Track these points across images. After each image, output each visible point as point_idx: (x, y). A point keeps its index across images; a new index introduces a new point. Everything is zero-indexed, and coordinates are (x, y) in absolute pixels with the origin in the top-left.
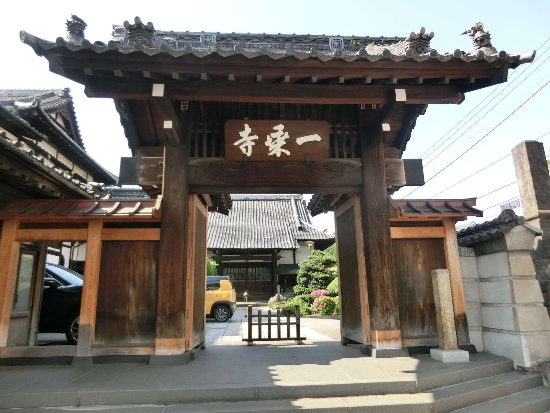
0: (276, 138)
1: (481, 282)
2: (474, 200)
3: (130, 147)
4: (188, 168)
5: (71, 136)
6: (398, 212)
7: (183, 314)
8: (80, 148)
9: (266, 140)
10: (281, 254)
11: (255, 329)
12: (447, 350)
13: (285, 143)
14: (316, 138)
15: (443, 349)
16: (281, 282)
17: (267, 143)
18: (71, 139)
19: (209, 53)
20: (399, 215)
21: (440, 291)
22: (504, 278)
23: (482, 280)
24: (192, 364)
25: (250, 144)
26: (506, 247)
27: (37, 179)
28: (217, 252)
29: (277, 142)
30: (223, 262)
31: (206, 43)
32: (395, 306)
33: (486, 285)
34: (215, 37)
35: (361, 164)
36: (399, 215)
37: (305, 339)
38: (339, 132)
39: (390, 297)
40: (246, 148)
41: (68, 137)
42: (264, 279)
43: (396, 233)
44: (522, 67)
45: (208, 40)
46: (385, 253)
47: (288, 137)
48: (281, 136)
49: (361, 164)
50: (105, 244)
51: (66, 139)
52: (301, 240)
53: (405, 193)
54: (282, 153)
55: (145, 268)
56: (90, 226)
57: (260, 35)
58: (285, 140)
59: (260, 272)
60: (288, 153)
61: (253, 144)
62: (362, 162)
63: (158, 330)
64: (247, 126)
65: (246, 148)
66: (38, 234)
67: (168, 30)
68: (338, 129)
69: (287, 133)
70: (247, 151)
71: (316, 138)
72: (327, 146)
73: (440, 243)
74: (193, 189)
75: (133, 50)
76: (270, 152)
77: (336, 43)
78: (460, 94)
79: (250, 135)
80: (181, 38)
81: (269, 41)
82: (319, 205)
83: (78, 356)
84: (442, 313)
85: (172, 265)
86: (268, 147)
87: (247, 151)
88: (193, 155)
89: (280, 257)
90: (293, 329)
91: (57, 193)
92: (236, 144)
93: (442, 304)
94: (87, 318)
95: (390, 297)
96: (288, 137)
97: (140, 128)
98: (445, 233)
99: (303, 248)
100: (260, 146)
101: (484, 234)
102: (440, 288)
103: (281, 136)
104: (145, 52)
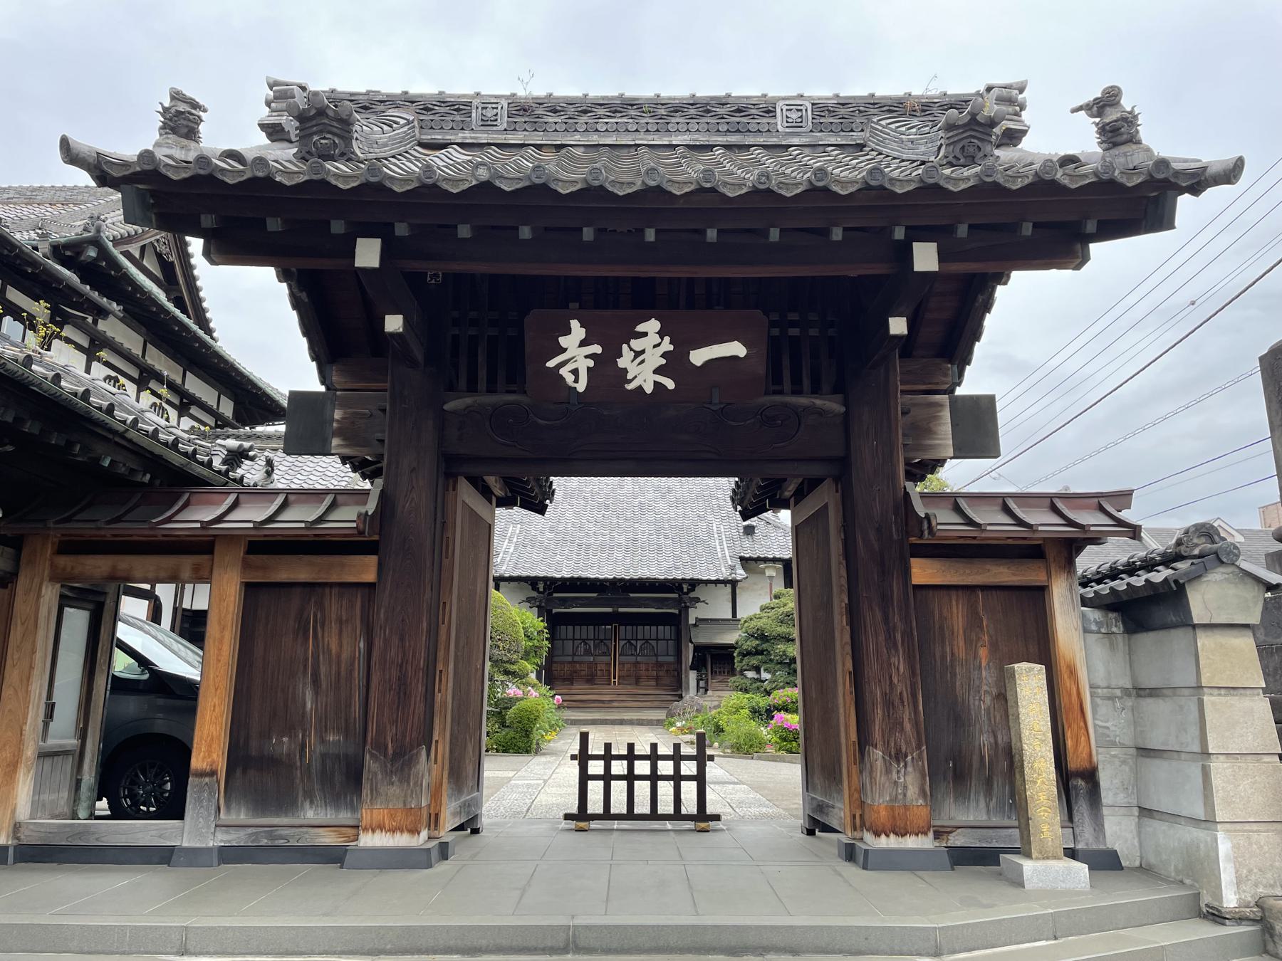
0: (643, 352)
1: (1139, 696)
2: (1124, 497)
3: (313, 359)
4: (442, 419)
5: (179, 303)
6: (926, 526)
7: (424, 752)
8: (201, 333)
9: (621, 356)
10: (699, 592)
11: (595, 788)
12: (1038, 859)
13: (663, 361)
14: (736, 349)
15: (1028, 855)
16: (698, 665)
17: (622, 363)
18: (177, 312)
19: (474, 183)
20: (926, 532)
21: (1022, 717)
22: (1186, 692)
23: (1141, 692)
24: (442, 868)
25: (584, 365)
26: (1191, 618)
27: (99, 448)
28: (541, 586)
29: (645, 360)
30: (554, 611)
31: (486, 123)
32: (919, 747)
33: (1149, 704)
34: (505, 106)
35: (843, 409)
36: (926, 532)
37: (717, 818)
38: (794, 332)
39: (908, 726)
40: (575, 372)
41: (170, 306)
42: (656, 655)
43: (923, 572)
44: (1214, 194)
45: (489, 113)
46: (896, 619)
47: (671, 348)
48: (655, 346)
49: (843, 409)
50: (251, 590)
51: (167, 312)
52: (750, 559)
53: (958, 475)
54: (656, 383)
55: (340, 642)
56: (217, 548)
57: (613, 98)
58: (664, 355)
59: (647, 637)
60: (670, 384)
61: (591, 363)
62: (846, 404)
63: (366, 791)
64: (575, 324)
65: (575, 372)
66: (98, 566)
67: (397, 90)
68: (793, 324)
69: (667, 339)
70: (576, 381)
71: (736, 349)
72: (761, 369)
73: (1039, 594)
74: (452, 467)
75: (306, 178)
76: (630, 381)
77: (794, 116)
78: (1079, 246)
79: (583, 344)
80: (427, 109)
81: (632, 112)
82: (755, 496)
83: (185, 844)
84: (1027, 771)
85: (402, 639)
86: (625, 371)
87: (576, 381)
88: (451, 388)
89: (698, 600)
90: (689, 789)
91: (144, 475)
92: (551, 364)
93: (1025, 747)
94: (209, 745)
95: (908, 726)
96: (671, 348)
97: (332, 319)
98: (1049, 576)
99: (753, 578)
100: (605, 369)
101: (1138, 581)
102: (1022, 710)
103: (655, 346)
104: (334, 182)
